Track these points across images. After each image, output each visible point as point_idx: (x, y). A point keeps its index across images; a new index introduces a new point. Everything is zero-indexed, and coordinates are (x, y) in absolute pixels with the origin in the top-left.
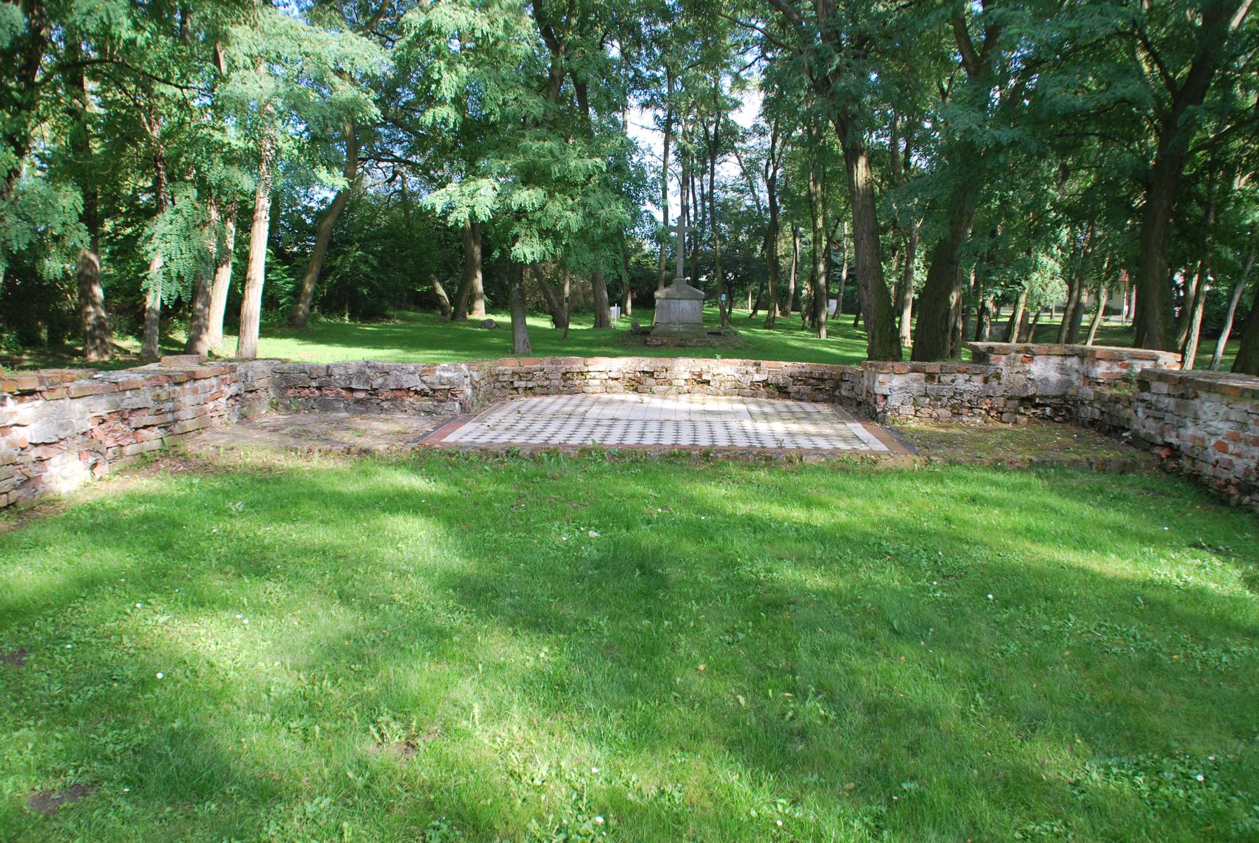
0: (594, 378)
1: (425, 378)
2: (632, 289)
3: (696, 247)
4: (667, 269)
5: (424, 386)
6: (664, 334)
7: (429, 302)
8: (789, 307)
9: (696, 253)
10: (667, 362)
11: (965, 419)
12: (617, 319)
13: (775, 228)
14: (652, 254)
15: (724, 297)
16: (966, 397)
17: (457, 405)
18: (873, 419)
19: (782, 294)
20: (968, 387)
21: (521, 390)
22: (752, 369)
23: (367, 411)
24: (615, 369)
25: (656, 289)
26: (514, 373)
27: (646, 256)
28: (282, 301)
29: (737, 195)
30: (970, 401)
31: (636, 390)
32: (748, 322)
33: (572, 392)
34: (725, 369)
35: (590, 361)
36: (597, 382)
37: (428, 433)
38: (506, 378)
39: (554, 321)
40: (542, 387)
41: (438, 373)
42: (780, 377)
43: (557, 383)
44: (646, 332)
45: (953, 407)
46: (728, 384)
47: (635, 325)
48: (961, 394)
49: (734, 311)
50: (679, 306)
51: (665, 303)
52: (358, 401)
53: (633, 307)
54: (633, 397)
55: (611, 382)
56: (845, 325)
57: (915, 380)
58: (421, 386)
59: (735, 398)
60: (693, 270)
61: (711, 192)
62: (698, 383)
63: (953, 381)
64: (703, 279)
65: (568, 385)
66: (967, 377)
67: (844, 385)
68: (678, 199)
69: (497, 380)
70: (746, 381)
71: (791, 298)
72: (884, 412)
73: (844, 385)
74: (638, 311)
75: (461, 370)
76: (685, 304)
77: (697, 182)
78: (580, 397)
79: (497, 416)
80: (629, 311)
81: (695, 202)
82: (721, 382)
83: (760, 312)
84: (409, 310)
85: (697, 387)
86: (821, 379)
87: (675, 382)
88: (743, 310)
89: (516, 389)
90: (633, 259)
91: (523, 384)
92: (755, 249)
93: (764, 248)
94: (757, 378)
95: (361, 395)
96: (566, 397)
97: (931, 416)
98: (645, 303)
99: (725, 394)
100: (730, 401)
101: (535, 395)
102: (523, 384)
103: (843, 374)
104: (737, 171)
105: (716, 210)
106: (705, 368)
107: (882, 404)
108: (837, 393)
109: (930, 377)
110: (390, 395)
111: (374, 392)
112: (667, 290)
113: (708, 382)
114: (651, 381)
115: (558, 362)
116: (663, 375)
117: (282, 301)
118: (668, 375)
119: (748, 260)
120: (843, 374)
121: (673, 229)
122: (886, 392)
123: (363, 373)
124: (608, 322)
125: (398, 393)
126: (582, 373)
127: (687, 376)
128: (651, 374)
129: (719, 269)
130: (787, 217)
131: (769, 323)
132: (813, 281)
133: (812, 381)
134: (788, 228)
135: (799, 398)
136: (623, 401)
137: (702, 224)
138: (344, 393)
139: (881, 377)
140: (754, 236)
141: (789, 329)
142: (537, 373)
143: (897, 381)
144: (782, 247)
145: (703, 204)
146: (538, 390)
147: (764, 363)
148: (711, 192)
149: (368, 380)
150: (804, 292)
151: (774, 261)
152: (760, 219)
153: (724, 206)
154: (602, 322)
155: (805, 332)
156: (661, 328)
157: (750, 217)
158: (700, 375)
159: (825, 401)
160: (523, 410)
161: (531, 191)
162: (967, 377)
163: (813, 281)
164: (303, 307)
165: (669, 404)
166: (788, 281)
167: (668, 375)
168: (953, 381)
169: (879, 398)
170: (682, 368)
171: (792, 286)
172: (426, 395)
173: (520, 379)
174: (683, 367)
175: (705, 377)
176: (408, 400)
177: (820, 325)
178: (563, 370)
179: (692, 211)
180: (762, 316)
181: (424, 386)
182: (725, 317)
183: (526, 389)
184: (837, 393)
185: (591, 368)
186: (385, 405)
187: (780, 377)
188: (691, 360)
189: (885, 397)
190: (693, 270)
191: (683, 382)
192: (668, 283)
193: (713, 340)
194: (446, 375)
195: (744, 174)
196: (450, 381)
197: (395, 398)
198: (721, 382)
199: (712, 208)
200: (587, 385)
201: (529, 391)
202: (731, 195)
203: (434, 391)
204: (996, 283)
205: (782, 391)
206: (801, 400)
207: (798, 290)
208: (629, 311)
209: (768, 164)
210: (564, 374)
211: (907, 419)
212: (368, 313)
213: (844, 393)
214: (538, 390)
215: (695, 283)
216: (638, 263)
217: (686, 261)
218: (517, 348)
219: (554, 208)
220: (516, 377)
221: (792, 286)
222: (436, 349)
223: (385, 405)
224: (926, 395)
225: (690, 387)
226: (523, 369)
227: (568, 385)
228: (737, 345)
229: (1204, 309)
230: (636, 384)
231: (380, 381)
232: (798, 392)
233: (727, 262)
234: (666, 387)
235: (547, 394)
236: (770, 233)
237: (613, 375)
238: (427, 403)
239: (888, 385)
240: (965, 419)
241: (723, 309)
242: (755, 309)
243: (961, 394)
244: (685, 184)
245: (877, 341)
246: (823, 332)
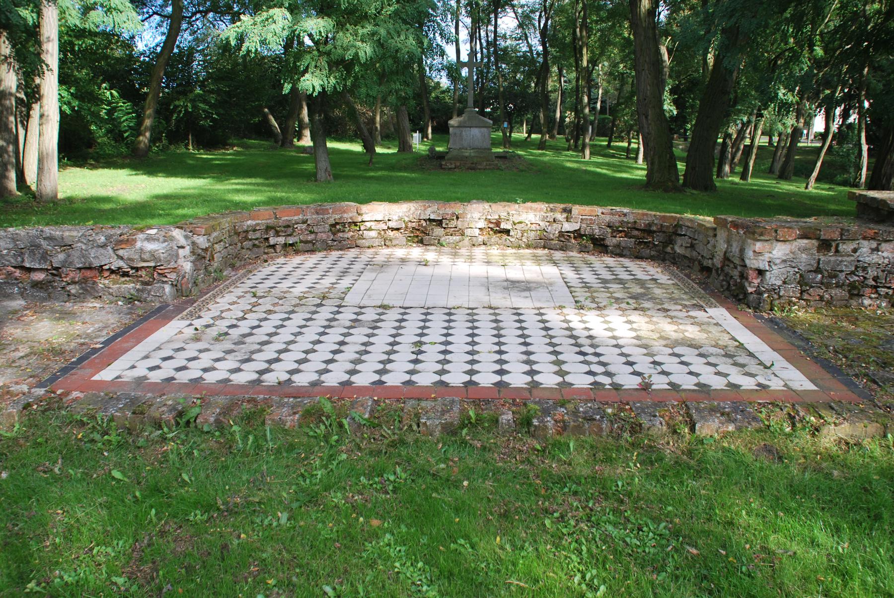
0: (370, 229)
1: (121, 252)
2: (432, 119)
3: (483, 84)
4: (460, 102)
5: (121, 264)
6: (456, 159)
7: (263, 131)
8: (555, 132)
9: (482, 89)
10: (458, 208)
11: (867, 302)
12: (417, 143)
13: (545, 68)
14: (448, 90)
15: (506, 124)
16: (872, 273)
17: (168, 288)
18: (739, 301)
19: (550, 120)
20: (875, 258)
21: (278, 248)
22: (560, 217)
23: (49, 297)
24: (395, 218)
25: (451, 118)
26: (268, 228)
27: (443, 92)
28: (126, 135)
29: (514, 43)
30: (875, 279)
31: (421, 242)
32: (524, 144)
33: (343, 246)
34: (530, 215)
35: (364, 208)
36: (373, 234)
37: (95, 351)
38: (258, 235)
39: (365, 146)
40: (306, 242)
41: (139, 244)
42: (595, 227)
43: (324, 236)
44: (441, 156)
45: (852, 286)
46: (532, 235)
47: (432, 150)
48: (864, 269)
49: (513, 135)
50: (471, 134)
51: (457, 131)
52: (36, 285)
53: (432, 133)
54: (416, 252)
55: (391, 234)
56: (601, 146)
57: (804, 250)
58: (117, 264)
59: (540, 252)
60: (481, 102)
61: (495, 39)
62: (496, 232)
63: (855, 251)
64: (488, 110)
65: (339, 237)
66: (874, 244)
67: (679, 241)
68: (468, 46)
69: (246, 239)
70: (554, 230)
71: (557, 125)
72: (759, 293)
73: (679, 241)
74: (437, 136)
75: (172, 239)
76: (475, 132)
77: (483, 34)
78: (352, 253)
79: (223, 301)
80: (430, 136)
81: (481, 48)
82: (523, 232)
83: (533, 136)
84: (250, 138)
85: (495, 238)
86: (648, 231)
87: (468, 232)
88: (520, 134)
89: (273, 246)
90: (433, 95)
91: (281, 240)
92: (529, 86)
93: (536, 85)
94: (568, 227)
95: (40, 276)
96: (335, 254)
97: (821, 298)
98: (442, 130)
99: (528, 246)
100: (537, 259)
101: (297, 252)
102: (281, 240)
103: (678, 226)
104: (515, 23)
105: (497, 52)
106: (503, 215)
107: (756, 282)
108: (669, 249)
109: (825, 245)
110: (78, 276)
111: (56, 271)
112: (460, 119)
113: (507, 232)
114: (439, 231)
115: (325, 212)
116: (453, 223)
117: (126, 135)
118: (459, 224)
119: (524, 95)
120: (678, 226)
121: (464, 65)
122: (763, 265)
123: (39, 246)
124: (410, 147)
125: (88, 273)
126: (355, 224)
127: (482, 224)
128: (439, 223)
129: (502, 102)
130: (556, 60)
131: (542, 145)
132: (578, 111)
133: (636, 233)
134: (555, 69)
135: (619, 252)
136: (403, 261)
137: (487, 66)
138: (18, 273)
139: (758, 246)
140: (528, 75)
141: (557, 149)
142: (299, 226)
143: (779, 251)
144: (551, 84)
145: (488, 49)
146: (301, 246)
147: (576, 209)
148: (495, 39)
149: (45, 256)
150: (567, 120)
151: (546, 95)
152: (533, 61)
153: (505, 50)
154: (405, 147)
155: (571, 152)
156: (454, 153)
157: (527, 60)
158: (498, 223)
159: (652, 258)
160: (261, 290)
161: (319, 20)
162: (874, 244)
163: (578, 111)
164: (144, 139)
165: (462, 268)
166: (555, 111)
167: (459, 224)
168: (855, 251)
169: (752, 274)
170: (476, 215)
171: (558, 115)
172: (126, 274)
173: (277, 234)
174: (477, 215)
175: (503, 226)
176: (102, 283)
177: (584, 146)
178: (332, 221)
179: (479, 55)
180: (535, 139)
181: (121, 264)
182: (507, 141)
183: (285, 245)
184: (669, 249)
185: (366, 217)
186: (73, 289)
187: (595, 227)
188: (486, 205)
189: (761, 272)
190: (481, 102)
191: (477, 232)
192: (460, 114)
193: (500, 163)
194: (150, 246)
195: (520, 26)
196: (153, 255)
197: (85, 280)
198: (523, 232)
199: (495, 52)
200: (362, 237)
201: (290, 249)
202: (509, 42)
203: (137, 269)
204: (740, 111)
205: (599, 245)
206: (621, 256)
207: (562, 118)
208: (430, 136)
209: (540, 16)
210: (333, 225)
211: (790, 303)
212: (210, 140)
213: (678, 250)
214: (301, 246)
215: (482, 113)
216: (437, 97)
217: (475, 95)
218: (319, 176)
219: (345, 38)
220: (272, 233)
221: (558, 115)
222: (250, 176)
223: (73, 289)
224: (818, 270)
225: (485, 238)
226: (281, 222)
227: (339, 237)
228: (521, 167)
229: (866, 132)
230: (421, 234)
231: (61, 257)
232: (618, 246)
233: (509, 95)
234: (457, 238)
235: (312, 251)
236: (542, 73)
237: (392, 224)
238: (129, 287)
239: (767, 255)
240: (867, 302)
241: (504, 134)
242: (530, 133)
243: (864, 269)
244: (473, 36)
245: (656, 167)
246: (587, 152)
